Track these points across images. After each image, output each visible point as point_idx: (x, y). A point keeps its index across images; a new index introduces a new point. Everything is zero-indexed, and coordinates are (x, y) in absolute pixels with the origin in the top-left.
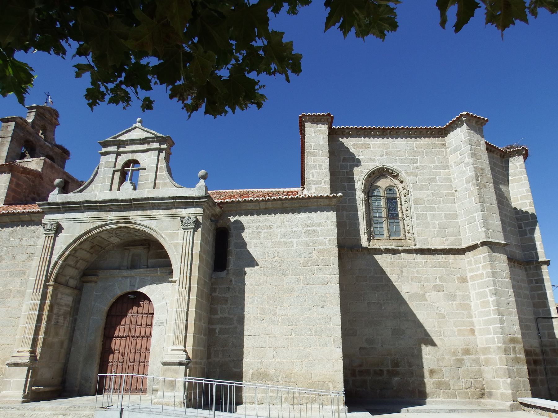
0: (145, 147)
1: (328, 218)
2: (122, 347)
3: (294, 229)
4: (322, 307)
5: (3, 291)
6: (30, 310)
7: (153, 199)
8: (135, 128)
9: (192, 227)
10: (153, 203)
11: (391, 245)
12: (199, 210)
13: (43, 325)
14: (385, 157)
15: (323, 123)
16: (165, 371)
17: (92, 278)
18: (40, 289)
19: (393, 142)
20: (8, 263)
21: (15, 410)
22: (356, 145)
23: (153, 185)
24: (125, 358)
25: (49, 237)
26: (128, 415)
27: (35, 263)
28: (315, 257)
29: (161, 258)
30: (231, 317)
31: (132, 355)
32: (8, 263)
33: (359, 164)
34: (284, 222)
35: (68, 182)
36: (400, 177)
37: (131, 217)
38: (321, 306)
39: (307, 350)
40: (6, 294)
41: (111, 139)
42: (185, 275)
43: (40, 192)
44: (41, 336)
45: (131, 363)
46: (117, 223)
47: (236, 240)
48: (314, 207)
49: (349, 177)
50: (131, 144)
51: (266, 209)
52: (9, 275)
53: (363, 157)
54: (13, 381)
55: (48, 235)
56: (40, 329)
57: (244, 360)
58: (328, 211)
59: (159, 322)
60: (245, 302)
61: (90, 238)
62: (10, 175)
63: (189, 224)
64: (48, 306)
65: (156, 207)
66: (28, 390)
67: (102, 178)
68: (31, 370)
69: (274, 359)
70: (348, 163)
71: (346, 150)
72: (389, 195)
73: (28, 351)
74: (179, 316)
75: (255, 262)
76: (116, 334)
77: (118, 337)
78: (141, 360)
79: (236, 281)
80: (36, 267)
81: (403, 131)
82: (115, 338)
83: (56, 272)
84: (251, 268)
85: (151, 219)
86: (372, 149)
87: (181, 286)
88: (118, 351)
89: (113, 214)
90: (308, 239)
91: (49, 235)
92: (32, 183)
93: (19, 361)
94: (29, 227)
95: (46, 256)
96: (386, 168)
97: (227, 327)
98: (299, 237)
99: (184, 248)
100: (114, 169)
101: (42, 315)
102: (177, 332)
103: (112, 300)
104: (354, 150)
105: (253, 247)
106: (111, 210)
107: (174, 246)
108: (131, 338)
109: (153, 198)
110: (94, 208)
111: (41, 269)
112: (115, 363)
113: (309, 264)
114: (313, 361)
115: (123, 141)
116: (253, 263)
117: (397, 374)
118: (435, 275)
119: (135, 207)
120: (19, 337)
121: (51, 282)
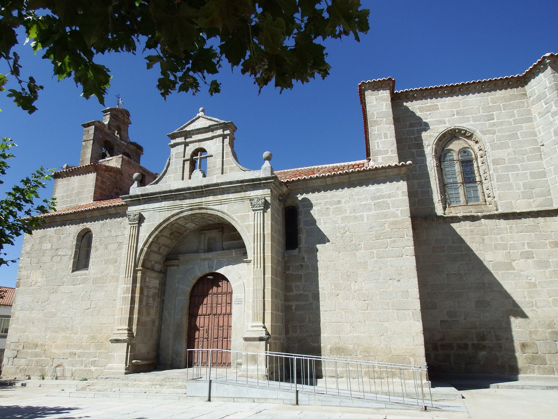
0: (210, 135)
2: (206, 324)
3: (364, 203)
4: (399, 281)
5: (101, 277)
7: (222, 184)
8: (199, 117)
9: (261, 208)
10: (223, 188)
11: (469, 211)
12: (267, 191)
13: (137, 306)
14: (455, 116)
16: (247, 346)
17: (174, 262)
18: (131, 274)
19: (464, 99)
21: (120, 380)
22: (422, 107)
23: (221, 171)
24: (210, 334)
25: (134, 227)
27: (124, 251)
30: (307, 293)
31: (216, 331)
34: (353, 196)
36: (475, 137)
37: (203, 203)
38: (397, 279)
39: (385, 324)
42: (259, 255)
43: (121, 187)
44: (136, 316)
46: (191, 210)
49: (418, 143)
51: (333, 184)
53: (431, 120)
55: (132, 226)
56: (134, 309)
58: (398, 181)
62: (95, 174)
68: (268, 345)
69: (351, 334)
71: (412, 114)
73: (126, 329)
75: (326, 239)
76: (200, 312)
78: (224, 337)
79: (308, 258)
80: (126, 254)
82: (199, 317)
84: (322, 245)
85: (222, 203)
87: (256, 266)
88: (203, 328)
89: (188, 201)
92: (114, 180)
93: (120, 338)
95: (133, 244)
96: (457, 129)
97: (303, 303)
99: (256, 229)
101: (135, 297)
104: (421, 113)
105: (322, 224)
108: (213, 316)
111: (130, 256)
112: (201, 339)
113: (382, 237)
114: (392, 335)
115: (189, 131)
116: (324, 239)
117: (484, 348)
118: (522, 241)
119: (207, 193)
121: (140, 268)
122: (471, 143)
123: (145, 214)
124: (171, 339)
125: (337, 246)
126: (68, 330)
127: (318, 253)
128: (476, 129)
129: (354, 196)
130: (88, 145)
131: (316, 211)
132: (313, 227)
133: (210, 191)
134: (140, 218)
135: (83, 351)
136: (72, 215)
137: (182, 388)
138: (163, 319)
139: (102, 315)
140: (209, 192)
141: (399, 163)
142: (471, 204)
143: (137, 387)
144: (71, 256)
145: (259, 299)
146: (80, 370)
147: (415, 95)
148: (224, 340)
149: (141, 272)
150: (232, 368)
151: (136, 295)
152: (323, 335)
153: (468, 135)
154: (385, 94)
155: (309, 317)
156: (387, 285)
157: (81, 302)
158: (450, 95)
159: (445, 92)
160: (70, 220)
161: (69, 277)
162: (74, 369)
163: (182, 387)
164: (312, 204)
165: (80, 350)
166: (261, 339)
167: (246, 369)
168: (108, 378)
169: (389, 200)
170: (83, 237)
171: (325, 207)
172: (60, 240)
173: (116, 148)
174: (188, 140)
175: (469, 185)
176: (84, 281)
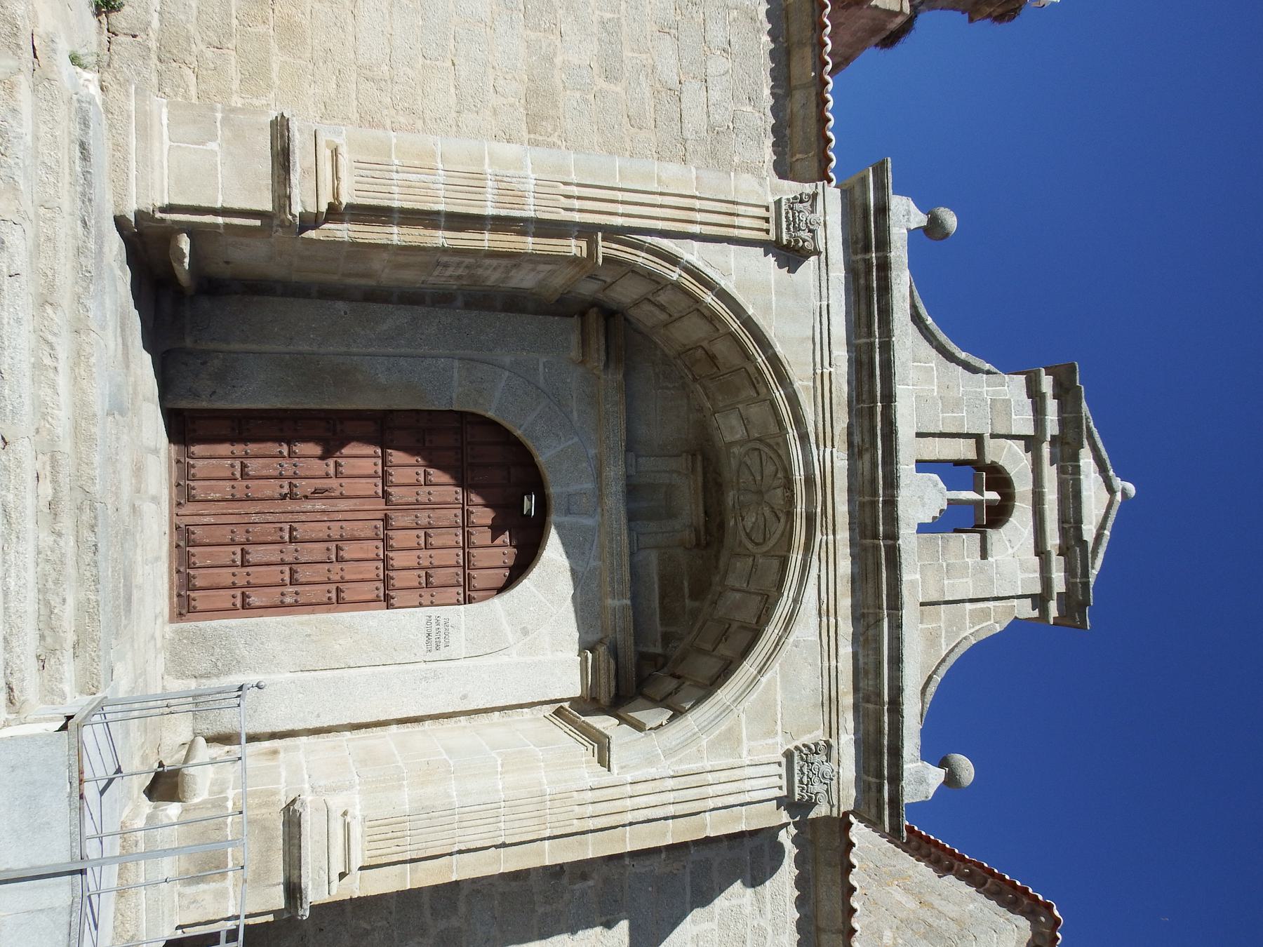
0: (1053, 540)
2: (350, 486)
6: (498, 179)
7: (896, 626)
8: (1111, 490)
9: (797, 790)
10: (879, 621)
16: (264, 828)
17: (598, 350)
18: (580, 211)
20: (648, 10)
21: (75, 237)
24: (308, 506)
25: (767, 220)
26: (53, 909)
29: (663, 597)
30: (462, 908)
31: (320, 530)
32: (648, 10)
37: (831, 537)
42: (629, 803)
44: (397, 235)
45: (292, 529)
46: (809, 481)
50: (1062, 485)
52: (608, 15)
54: (214, 153)
56: (426, 227)
59: (442, 630)
61: (751, 370)
63: (805, 780)
64: (512, 245)
65: (861, 630)
66: (175, 222)
68: (258, 223)
73: (336, 194)
76: (397, 456)
77: (384, 464)
80: (659, 182)
82: (379, 451)
83: (640, 260)
85: (824, 619)
87: (589, 796)
88: (332, 471)
91: (772, 221)
95: (699, 217)
99: (723, 776)
100: (987, 435)
107: (730, 730)
108: (380, 515)
109: (900, 626)
110: (866, 388)
112: (288, 469)
115: (1075, 458)
119: (864, 549)
120: (394, 141)
121: (604, 248)
127: (599, 929)
134: (798, 251)
137: (42, 637)
138: (375, 306)
143: (38, 366)
148: (286, 569)
149: (585, 255)
150: (170, 629)
151: (487, 235)
155: (373, 930)
163: (47, 633)
164: (762, 882)
166: (293, 891)
168: (85, 157)
174: (1046, 449)
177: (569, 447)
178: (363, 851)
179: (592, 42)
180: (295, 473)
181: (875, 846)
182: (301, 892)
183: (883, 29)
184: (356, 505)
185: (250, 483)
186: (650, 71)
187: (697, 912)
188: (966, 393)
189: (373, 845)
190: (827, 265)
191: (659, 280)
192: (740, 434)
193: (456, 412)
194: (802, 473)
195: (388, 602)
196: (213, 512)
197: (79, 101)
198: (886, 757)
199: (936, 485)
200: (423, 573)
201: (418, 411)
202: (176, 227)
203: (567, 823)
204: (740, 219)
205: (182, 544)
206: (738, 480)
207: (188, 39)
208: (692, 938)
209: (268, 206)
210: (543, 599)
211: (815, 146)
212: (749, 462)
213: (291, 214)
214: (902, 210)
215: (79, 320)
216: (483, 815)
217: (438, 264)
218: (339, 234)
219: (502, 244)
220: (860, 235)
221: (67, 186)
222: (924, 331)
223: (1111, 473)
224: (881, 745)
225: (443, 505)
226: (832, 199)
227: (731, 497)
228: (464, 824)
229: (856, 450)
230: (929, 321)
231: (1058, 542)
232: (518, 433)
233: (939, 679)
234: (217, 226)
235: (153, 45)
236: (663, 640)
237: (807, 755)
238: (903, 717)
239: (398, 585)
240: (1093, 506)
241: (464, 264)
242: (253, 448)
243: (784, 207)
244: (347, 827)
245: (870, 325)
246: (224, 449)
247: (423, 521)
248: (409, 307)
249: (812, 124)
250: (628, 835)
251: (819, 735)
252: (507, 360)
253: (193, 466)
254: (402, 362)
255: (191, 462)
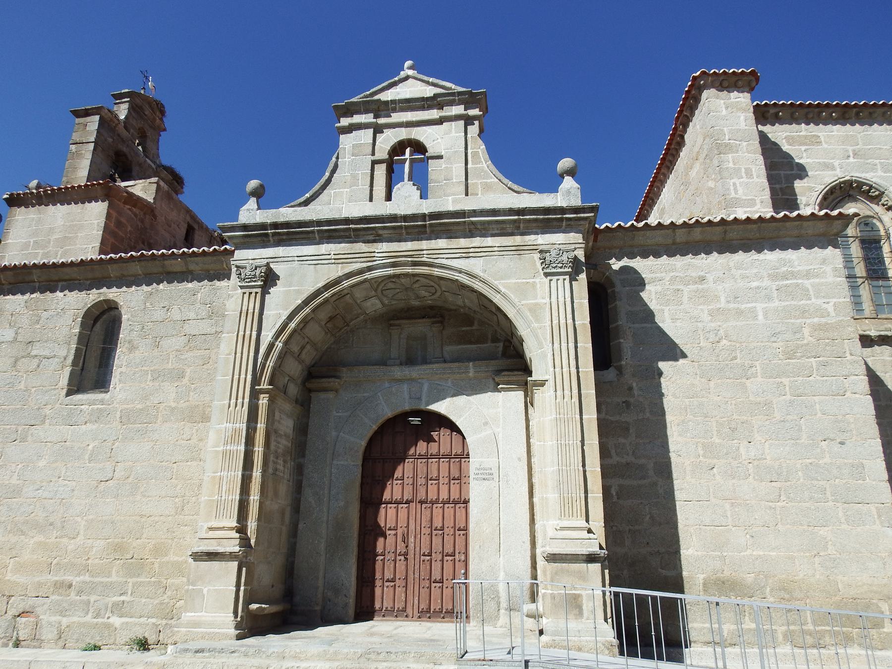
0: (434, 114)
1: (824, 261)
2: (402, 522)
3: (755, 284)
4: (842, 443)
5: (142, 410)
7: (474, 213)
8: (407, 78)
9: (566, 270)
10: (472, 223)
11: (886, 328)
12: (574, 238)
13: (257, 474)
14: (851, 160)
15: (740, 89)
16: (556, 573)
17: (329, 382)
18: (243, 398)
19: (863, 132)
20: (146, 354)
21: (239, 657)
22: (793, 137)
23: (463, 188)
24: (411, 545)
25: (250, 293)
27: (227, 345)
28: (808, 339)
29: (471, 343)
30: (642, 461)
31: (425, 539)
32: (146, 354)
33: (803, 173)
34: (730, 269)
35: (193, 229)
36: (886, 199)
37: (425, 252)
38: (839, 440)
39: (821, 532)
40: (148, 414)
41: (360, 98)
42: (565, 369)
43: (152, 241)
44: (254, 497)
45: (424, 555)
46: (394, 265)
47: (630, 306)
48: (791, 240)
49: (788, 199)
51: (687, 243)
53: (808, 160)
55: (247, 291)
56: (251, 482)
57: (682, 552)
58: (823, 247)
59: (482, 471)
60: (669, 432)
61: (334, 298)
62: (106, 204)
63: (560, 265)
64: (262, 435)
65: (478, 232)
66: (243, 611)
67: (350, 178)
68: (244, 569)
69: (749, 552)
70: (782, 173)
71: (774, 147)
72: (865, 234)
73: (231, 529)
74: (564, 457)
75: (678, 351)
76: (387, 496)
77: (391, 503)
78: (446, 551)
79: (641, 389)
80: (229, 354)
81: (885, 109)
82: (383, 506)
83: (271, 364)
84: (670, 363)
85: (471, 255)
86: (825, 146)
87: (559, 393)
88: (393, 532)
89: (384, 247)
90: (787, 303)
91: (251, 290)
92: (140, 224)
93: (218, 548)
94: (184, 283)
95: (248, 332)
96: (856, 181)
97: (635, 483)
98: (766, 299)
99: (555, 314)
100: (373, 158)
101: (252, 452)
102: (565, 489)
103: (374, 427)
104: (790, 147)
105: (668, 320)
106: (378, 238)
107: (530, 310)
108: (419, 505)
109: (474, 211)
110: (342, 234)
111: (242, 358)
113: (799, 355)
114: (838, 556)
115: (386, 103)
116: (674, 352)
120: (206, 498)
121: (264, 385)
122: (878, 209)
123: (276, 267)
124: (322, 553)
125: (703, 368)
126: (51, 527)
127: (662, 380)
128: (889, 186)
129: (733, 271)
130: (83, 152)
131: (653, 294)
132: (649, 325)
133: (443, 228)
134: (267, 275)
135: (92, 579)
136: (75, 269)
138: (302, 507)
139: (144, 496)
140: (440, 229)
141: (820, 210)
142: (884, 316)
144: (65, 359)
145: (572, 467)
146: (83, 625)
147: (780, 114)
148: (446, 558)
149: (268, 395)
151: (256, 449)
152: (684, 551)
153: (874, 194)
154: (742, 100)
155: (650, 513)
156: (819, 450)
157: (88, 464)
158: (841, 121)
159: (834, 114)
160: (65, 280)
161: (58, 405)
162: (65, 621)
164: (643, 279)
165: (82, 577)
166: (591, 558)
167: (565, 629)
169: (807, 283)
170: (96, 321)
171: (671, 287)
172: (38, 322)
173: (136, 169)
174: (382, 121)
175: (876, 282)
176: (98, 417)
177: (383, 399)
178: (577, 520)
179: (163, 386)
180: (393, 553)
181: (673, 184)
182: (591, 554)
183: (168, 192)
184: (412, 519)
185: (397, 577)
186: (179, 353)
187: (657, 319)
188: (348, 172)
189: (575, 514)
190: (276, 258)
191: (284, 353)
192: (375, 301)
193: (363, 462)
194: (389, 269)
195: (466, 502)
196: (412, 598)
197: (176, 653)
198: (550, 216)
199: (399, 189)
200: (452, 482)
201: (362, 484)
202: (246, 611)
203: (573, 405)
204: (250, 308)
205: (428, 615)
206: (404, 300)
207: (161, 604)
208: (673, 322)
209: (236, 563)
210: (468, 414)
211: (219, 257)
212: (391, 295)
213: (239, 552)
214: (247, 214)
215: (278, 656)
216: (564, 453)
217: (274, 474)
218: (253, 527)
219: (261, 441)
220: (259, 239)
221: (215, 660)
222: (313, 198)
223: (396, 79)
224: (544, 219)
225: (415, 470)
226: (240, 254)
227: (416, 303)
228: (568, 464)
229: (377, 238)
230: (308, 195)
231: (435, 110)
232: (375, 427)
233: (510, 182)
234: (245, 590)
235: (164, 622)
236: (495, 342)
237: (546, 265)
238: (526, 208)
239: (458, 496)
240: (416, 89)
241: (275, 460)
242: (378, 576)
243: (244, 284)
244: (563, 529)
245: (308, 232)
246: (378, 591)
247: (423, 481)
248: (302, 489)
249: (206, 259)
250: (584, 370)
251: (537, 256)
252: (334, 434)
253: (387, 608)
254: (333, 493)
255: (384, 609)
